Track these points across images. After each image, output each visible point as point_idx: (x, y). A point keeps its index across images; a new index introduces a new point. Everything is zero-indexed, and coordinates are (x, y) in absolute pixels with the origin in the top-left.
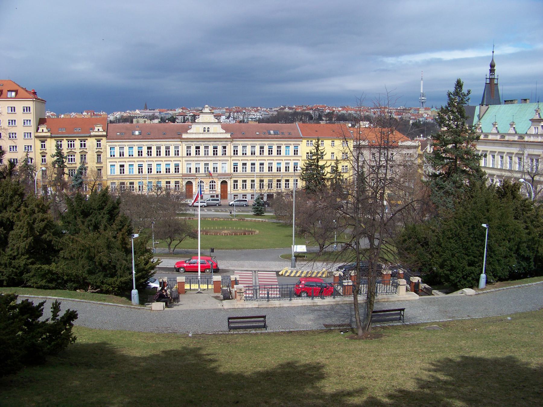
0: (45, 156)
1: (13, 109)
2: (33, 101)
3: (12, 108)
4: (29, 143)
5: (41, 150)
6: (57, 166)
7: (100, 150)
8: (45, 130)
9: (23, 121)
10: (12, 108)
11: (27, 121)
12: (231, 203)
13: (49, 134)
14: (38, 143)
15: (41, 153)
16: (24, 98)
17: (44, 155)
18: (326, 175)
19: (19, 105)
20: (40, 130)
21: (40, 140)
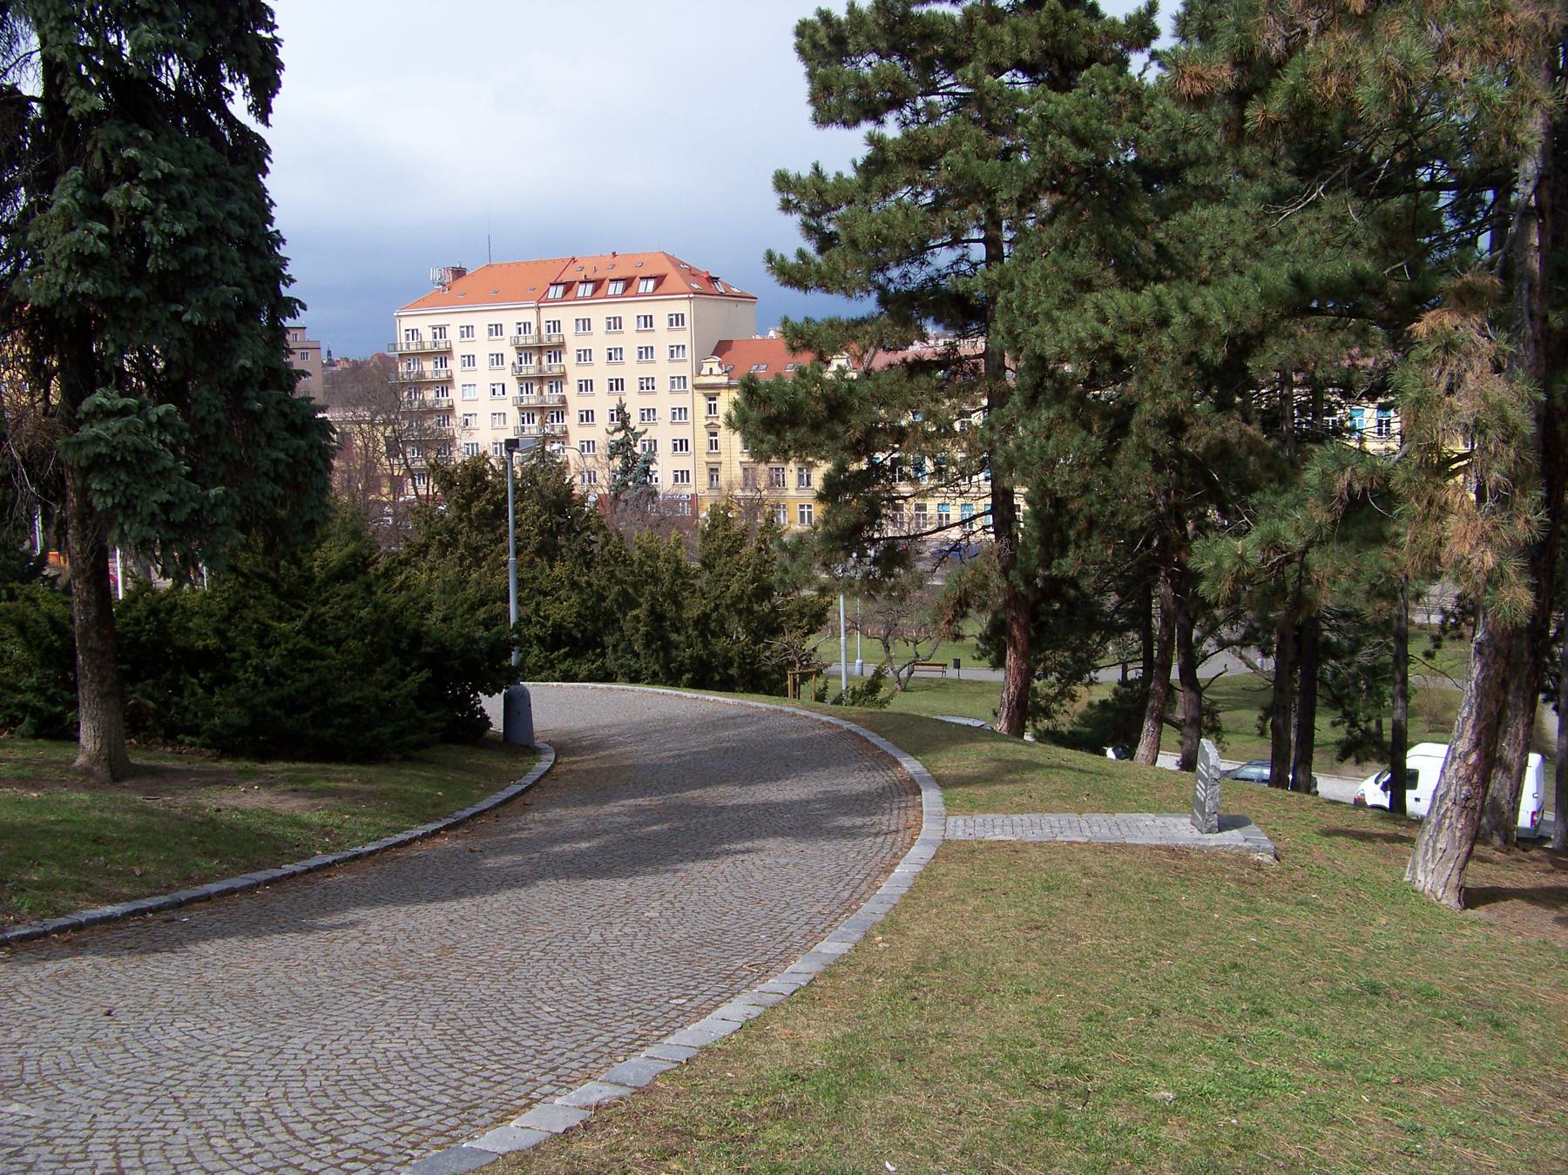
0: (715, 434)
1: (648, 321)
2: (690, 298)
3: (645, 317)
4: (683, 400)
5: (707, 418)
6: (810, 459)
7: (715, 421)
8: (717, 370)
9: (487, 327)
10: (645, 317)
11: (678, 347)
12: (1473, 497)
13: (724, 380)
14: (701, 402)
15: (706, 426)
16: (674, 294)
17: (713, 430)
18: (886, 701)
19: (661, 311)
20: (705, 371)
21: (705, 395)
